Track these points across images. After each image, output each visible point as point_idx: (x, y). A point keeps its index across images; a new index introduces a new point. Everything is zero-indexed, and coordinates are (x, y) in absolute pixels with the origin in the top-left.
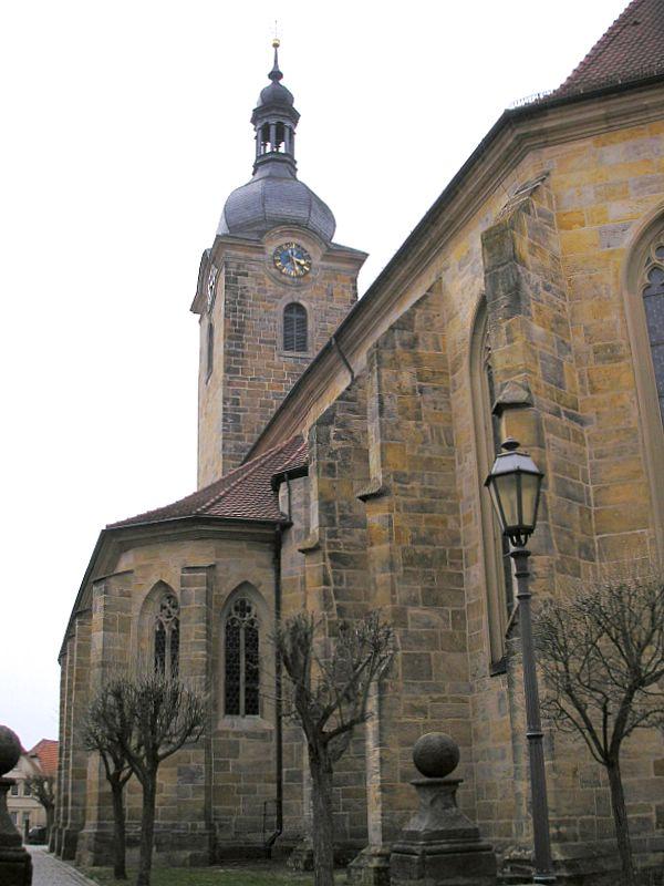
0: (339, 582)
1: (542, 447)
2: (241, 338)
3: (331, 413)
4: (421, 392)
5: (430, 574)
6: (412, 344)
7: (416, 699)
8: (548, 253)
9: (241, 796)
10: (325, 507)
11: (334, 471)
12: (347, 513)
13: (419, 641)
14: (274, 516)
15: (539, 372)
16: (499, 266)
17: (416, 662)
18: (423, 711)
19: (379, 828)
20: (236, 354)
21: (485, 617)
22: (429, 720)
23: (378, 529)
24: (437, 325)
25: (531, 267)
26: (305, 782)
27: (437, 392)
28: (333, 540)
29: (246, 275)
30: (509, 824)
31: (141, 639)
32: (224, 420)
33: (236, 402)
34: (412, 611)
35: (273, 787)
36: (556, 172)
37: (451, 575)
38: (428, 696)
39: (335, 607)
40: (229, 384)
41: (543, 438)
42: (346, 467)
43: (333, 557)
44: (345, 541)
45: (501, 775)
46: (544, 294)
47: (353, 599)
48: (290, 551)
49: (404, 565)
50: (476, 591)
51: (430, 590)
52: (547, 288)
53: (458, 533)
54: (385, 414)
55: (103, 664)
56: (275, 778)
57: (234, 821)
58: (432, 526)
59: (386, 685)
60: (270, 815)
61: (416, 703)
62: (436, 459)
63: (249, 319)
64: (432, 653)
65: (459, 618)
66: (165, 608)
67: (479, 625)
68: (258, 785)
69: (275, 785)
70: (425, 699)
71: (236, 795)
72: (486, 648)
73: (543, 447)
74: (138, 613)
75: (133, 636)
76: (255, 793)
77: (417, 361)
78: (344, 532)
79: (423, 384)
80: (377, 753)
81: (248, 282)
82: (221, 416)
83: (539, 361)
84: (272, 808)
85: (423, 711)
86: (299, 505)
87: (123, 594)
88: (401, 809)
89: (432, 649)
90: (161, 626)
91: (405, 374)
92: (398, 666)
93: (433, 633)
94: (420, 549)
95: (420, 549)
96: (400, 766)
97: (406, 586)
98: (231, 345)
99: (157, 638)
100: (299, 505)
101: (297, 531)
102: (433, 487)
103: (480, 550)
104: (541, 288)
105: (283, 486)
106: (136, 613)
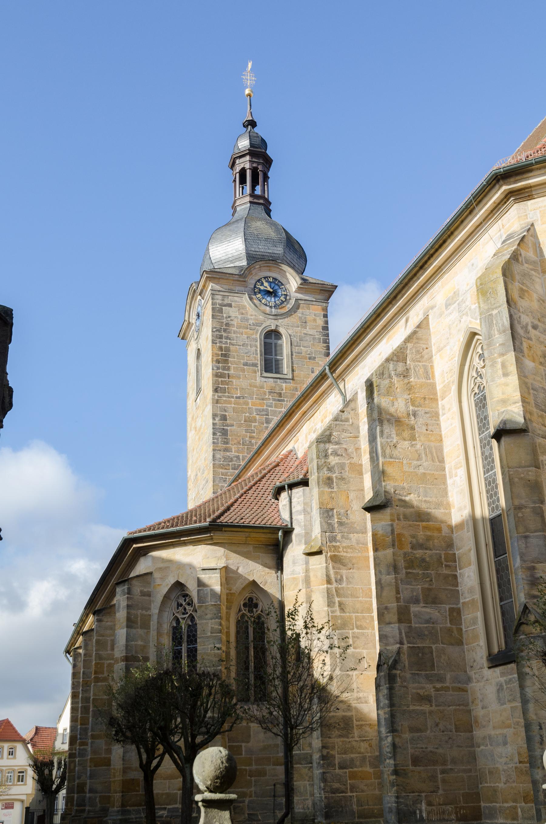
0: (339, 581)
1: (538, 467)
2: (226, 361)
3: (328, 433)
4: (415, 415)
5: (428, 576)
6: (405, 374)
7: (423, 688)
8: (535, 296)
9: (253, 778)
10: (326, 515)
11: (332, 483)
12: (344, 520)
13: (420, 635)
14: (271, 521)
15: (533, 402)
16: (493, 309)
17: (420, 655)
18: (427, 699)
19: (394, 810)
20: (221, 376)
21: (479, 615)
22: (434, 708)
23: (383, 536)
24: (426, 357)
25: (521, 310)
26: (315, 765)
27: (428, 415)
28: (334, 544)
29: (230, 305)
30: (515, 808)
31: (159, 634)
32: (214, 434)
33: (224, 418)
34: (414, 609)
35: (281, 769)
36: (540, 222)
37: (446, 577)
38: (431, 686)
39: (337, 604)
40: (217, 402)
41: (538, 459)
42: (342, 479)
43: (336, 559)
44: (344, 545)
45: (503, 760)
46: (533, 333)
47: (352, 596)
48: (294, 553)
49: (406, 568)
50: (471, 590)
51: (429, 590)
52: (535, 327)
53: (451, 539)
54: (384, 436)
55: (127, 659)
56: (283, 760)
57: (247, 802)
58: (429, 533)
59: (395, 675)
60: (279, 797)
61: (421, 692)
62: (429, 474)
63: (233, 345)
64: (434, 647)
65: (456, 615)
66: (181, 605)
67: (474, 621)
68: (268, 768)
69: (283, 767)
70: (429, 688)
71: (249, 778)
72: (482, 642)
73: (539, 468)
74: (157, 611)
75: (153, 633)
76: (265, 774)
77: (410, 388)
78: (343, 537)
79: (416, 409)
80: (390, 739)
81: (232, 312)
82: (210, 430)
83: (531, 391)
84: (281, 790)
85: (427, 699)
86: (299, 513)
87: (143, 594)
88: (413, 792)
89: (434, 644)
90: (177, 620)
91: (400, 400)
92: (405, 658)
93: (433, 628)
94: (419, 553)
95: (419, 553)
96: (410, 751)
97: (408, 586)
98: (218, 368)
99: (174, 633)
100: (299, 513)
101: (298, 535)
102: (428, 499)
103: (473, 555)
104: (530, 328)
105: (284, 495)
106: (155, 610)
